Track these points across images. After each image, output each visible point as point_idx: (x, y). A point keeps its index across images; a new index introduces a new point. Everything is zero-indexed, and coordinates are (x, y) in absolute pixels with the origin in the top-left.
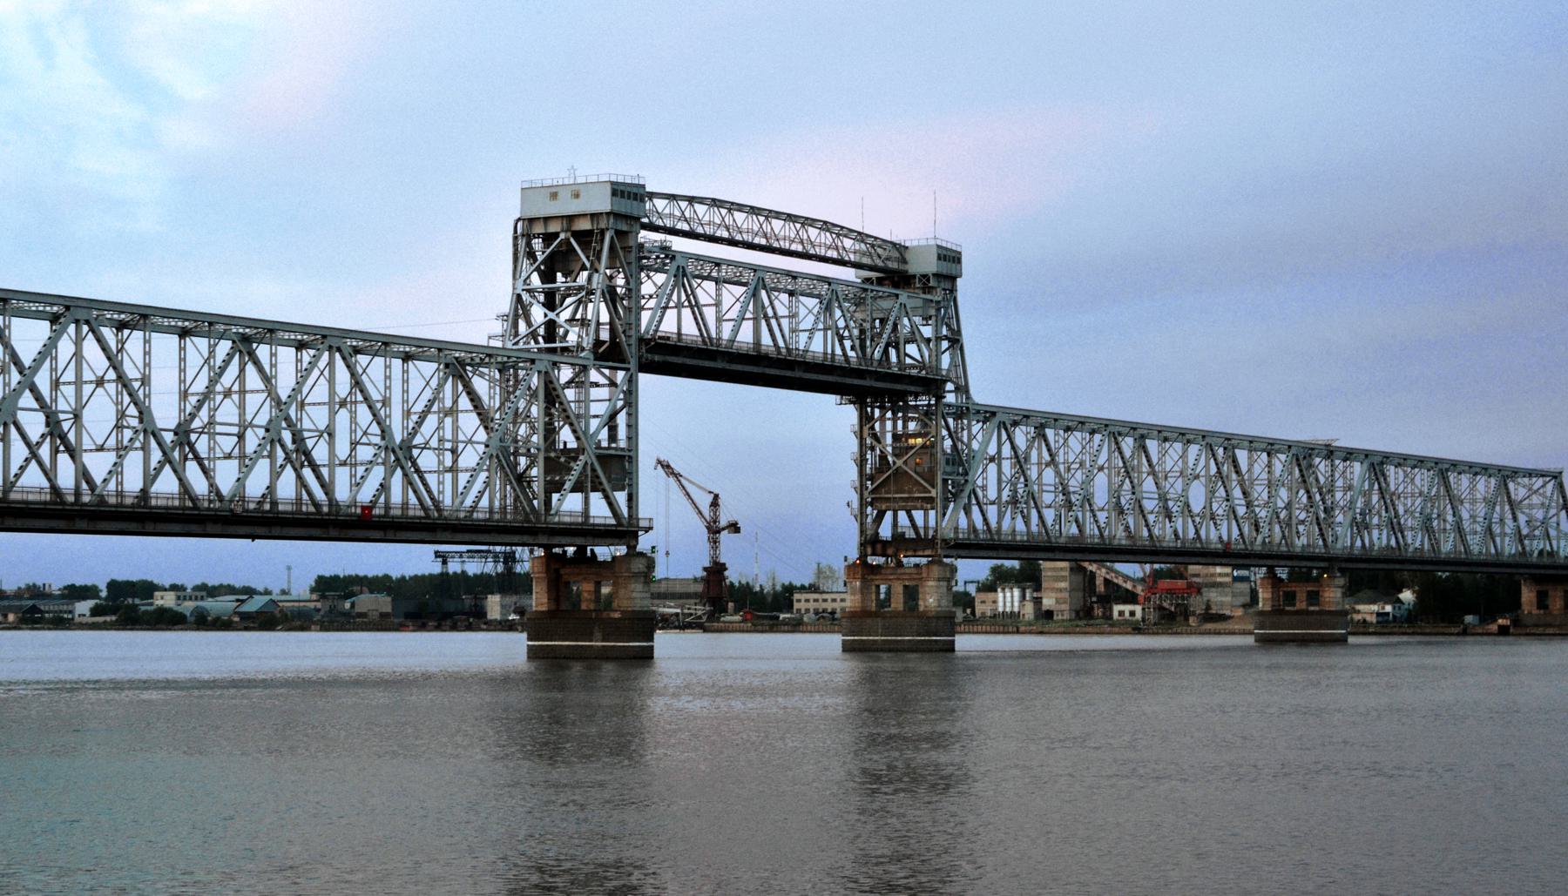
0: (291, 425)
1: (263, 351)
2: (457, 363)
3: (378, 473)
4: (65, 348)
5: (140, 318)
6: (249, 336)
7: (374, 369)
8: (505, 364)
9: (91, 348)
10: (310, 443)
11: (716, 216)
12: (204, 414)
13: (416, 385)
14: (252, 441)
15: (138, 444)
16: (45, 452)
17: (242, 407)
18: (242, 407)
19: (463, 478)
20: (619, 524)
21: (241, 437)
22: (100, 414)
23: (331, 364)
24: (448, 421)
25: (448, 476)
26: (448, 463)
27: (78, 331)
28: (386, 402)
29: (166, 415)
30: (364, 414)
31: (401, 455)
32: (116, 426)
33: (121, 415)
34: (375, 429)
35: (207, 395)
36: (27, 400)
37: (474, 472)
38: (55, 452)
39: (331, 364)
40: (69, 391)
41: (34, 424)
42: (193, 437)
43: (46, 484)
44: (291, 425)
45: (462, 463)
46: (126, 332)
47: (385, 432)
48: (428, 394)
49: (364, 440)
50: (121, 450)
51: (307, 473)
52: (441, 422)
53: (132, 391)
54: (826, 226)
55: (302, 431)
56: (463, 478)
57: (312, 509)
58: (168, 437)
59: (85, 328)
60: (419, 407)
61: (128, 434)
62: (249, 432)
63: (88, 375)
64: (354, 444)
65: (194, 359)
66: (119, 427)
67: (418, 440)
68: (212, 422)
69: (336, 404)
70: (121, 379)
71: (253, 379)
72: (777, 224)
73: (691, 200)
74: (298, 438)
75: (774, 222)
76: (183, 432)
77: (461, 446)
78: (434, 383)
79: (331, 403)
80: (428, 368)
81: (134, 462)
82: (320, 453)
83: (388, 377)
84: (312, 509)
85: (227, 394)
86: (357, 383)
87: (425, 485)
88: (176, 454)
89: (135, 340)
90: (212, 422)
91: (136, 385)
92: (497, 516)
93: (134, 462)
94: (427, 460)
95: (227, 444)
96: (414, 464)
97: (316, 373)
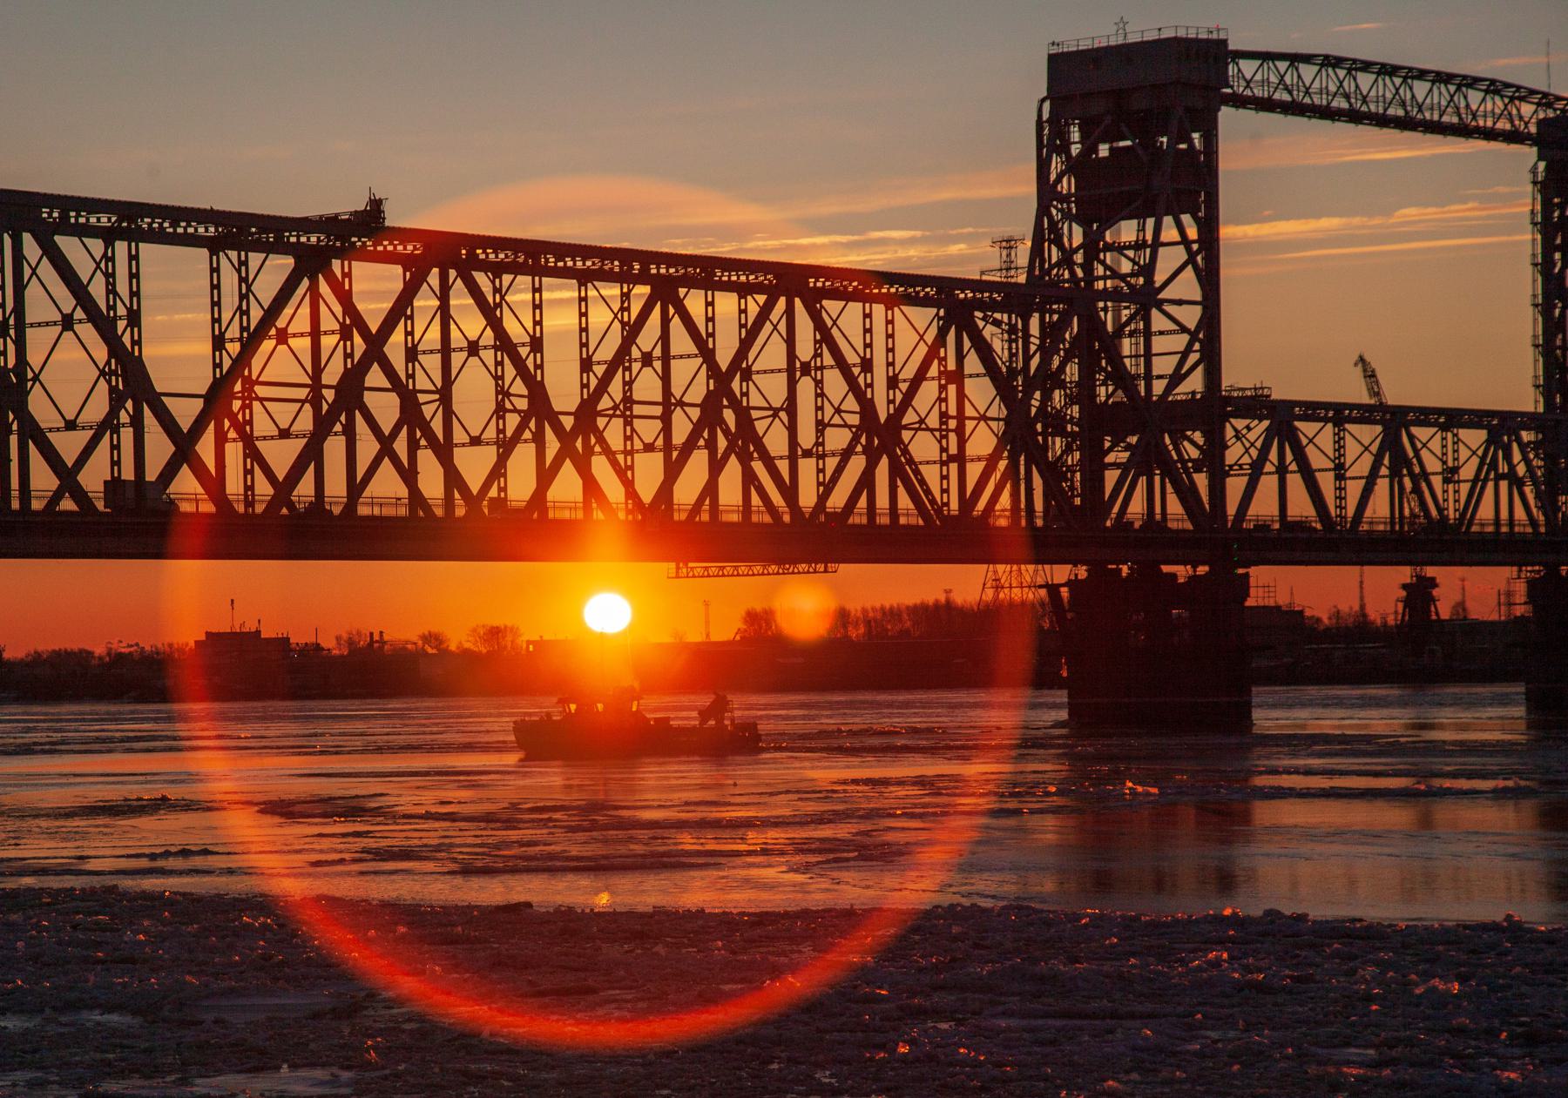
0: (735, 405)
1: (695, 302)
2: (955, 302)
3: (857, 464)
4: (425, 302)
5: (534, 258)
6: (668, 277)
7: (848, 318)
8: (1014, 300)
9: (460, 300)
10: (760, 427)
11: (1331, 80)
12: (616, 388)
13: (905, 339)
14: (681, 428)
15: (527, 435)
16: (401, 446)
17: (666, 378)
18: (666, 378)
19: (974, 471)
20: (1536, 532)
21: (666, 419)
22: (475, 389)
23: (790, 312)
24: (952, 388)
25: (954, 467)
26: (953, 450)
27: (444, 278)
28: (867, 365)
29: (565, 392)
30: (834, 383)
31: (881, 436)
32: (496, 412)
33: (502, 392)
34: (851, 404)
35: (621, 358)
36: (375, 377)
37: (846, 455)
38: (413, 447)
39: (790, 312)
40: (433, 363)
41: (385, 407)
42: (601, 422)
43: (403, 492)
44: (735, 405)
45: (971, 449)
46: (507, 278)
47: (867, 408)
48: (922, 350)
49: (837, 420)
50: (506, 447)
51: (758, 467)
52: (942, 388)
53: (518, 357)
54: (1494, 87)
55: (749, 408)
56: (974, 471)
57: (767, 519)
58: (568, 422)
59: (452, 273)
60: (909, 373)
61: (512, 421)
62: (678, 415)
63: (456, 339)
64: (821, 426)
65: (600, 317)
66: (500, 411)
67: (910, 417)
68: (628, 400)
69: (794, 369)
70: (504, 343)
71: (681, 341)
72: (1365, 80)
73: (1295, 59)
74: (743, 414)
75: (1360, 76)
76: (587, 412)
77: (969, 425)
78: (930, 336)
79: (791, 370)
80: (924, 317)
81: (523, 462)
82: (776, 441)
83: (868, 331)
84: (767, 519)
85: (647, 359)
86: (825, 337)
87: (922, 482)
88: (579, 444)
89: (519, 292)
90: (628, 400)
91: (524, 351)
92: (1504, 529)
93: (523, 462)
94: (923, 447)
95: (649, 430)
96: (906, 451)
97: (768, 327)
